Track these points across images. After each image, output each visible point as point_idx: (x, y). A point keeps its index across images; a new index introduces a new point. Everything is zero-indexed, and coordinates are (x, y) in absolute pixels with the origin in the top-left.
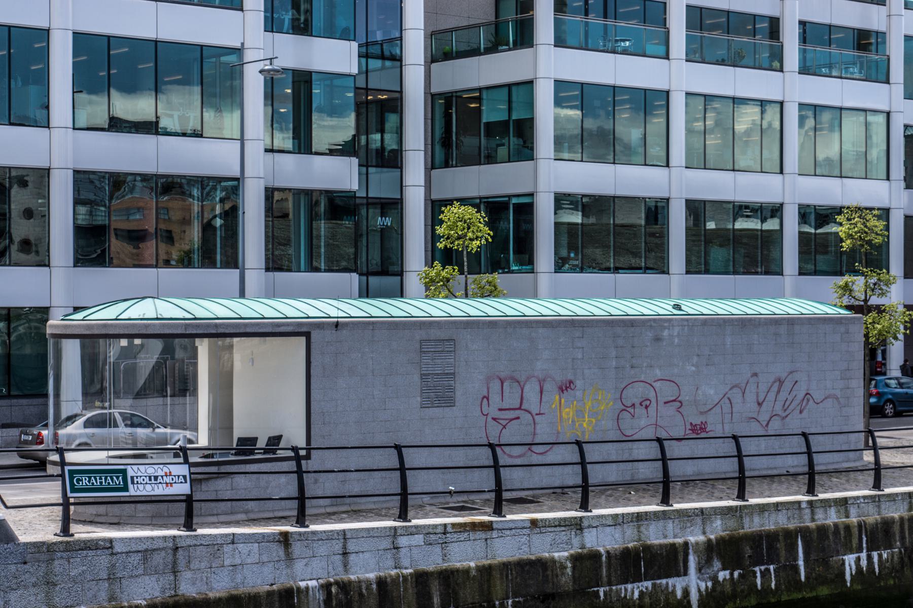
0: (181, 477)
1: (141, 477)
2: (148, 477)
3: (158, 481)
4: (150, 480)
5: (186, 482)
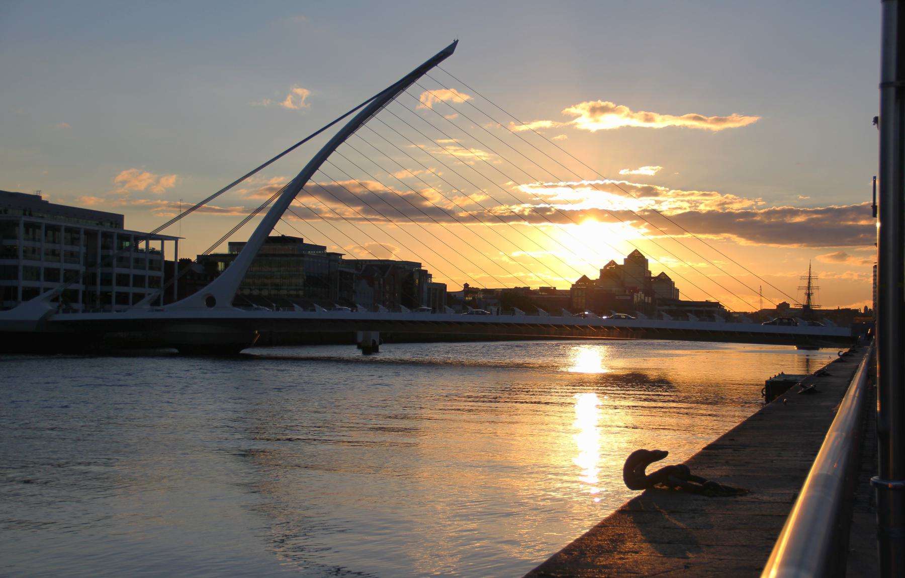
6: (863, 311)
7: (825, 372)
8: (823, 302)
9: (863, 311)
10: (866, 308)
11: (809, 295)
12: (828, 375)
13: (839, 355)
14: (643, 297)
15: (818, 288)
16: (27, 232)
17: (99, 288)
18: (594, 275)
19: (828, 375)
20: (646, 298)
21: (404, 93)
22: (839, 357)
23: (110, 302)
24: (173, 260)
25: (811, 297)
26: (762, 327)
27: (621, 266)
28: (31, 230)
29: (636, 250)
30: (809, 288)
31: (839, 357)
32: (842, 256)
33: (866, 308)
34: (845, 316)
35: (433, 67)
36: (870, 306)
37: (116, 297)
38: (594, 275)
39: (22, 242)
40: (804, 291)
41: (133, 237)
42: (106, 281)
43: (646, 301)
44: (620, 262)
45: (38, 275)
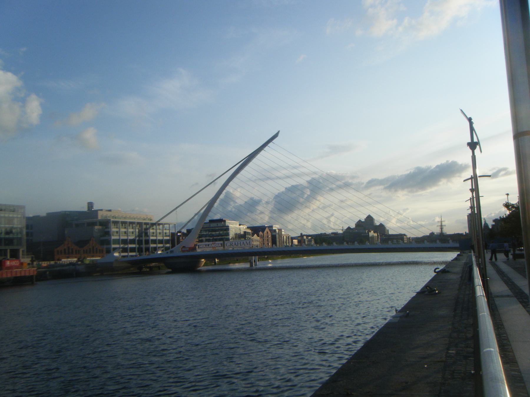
0: (220, 244)
1: (202, 245)
2: (205, 245)
3: (210, 246)
4: (206, 246)
5: (222, 246)
6: (464, 234)
7: (445, 269)
8: (449, 230)
9: (464, 234)
10: (466, 232)
11: (442, 229)
12: (448, 272)
13: (435, 272)
14: (373, 234)
15: (445, 225)
16: (122, 225)
17: (144, 246)
18: (353, 226)
19: (448, 272)
20: (375, 234)
21: (259, 155)
22: (436, 274)
23: (142, 251)
24: (174, 232)
25: (443, 229)
26: (427, 244)
27: (363, 222)
28: (124, 225)
29: (369, 215)
30: (441, 226)
31: (436, 274)
32: (447, 161)
33: (466, 232)
34: (456, 237)
35: (270, 143)
36: (467, 232)
37: (138, 249)
38: (353, 226)
39: (114, 229)
40: (439, 227)
41: (128, 222)
42: (147, 242)
43: (375, 235)
44: (363, 220)
45: (119, 242)
